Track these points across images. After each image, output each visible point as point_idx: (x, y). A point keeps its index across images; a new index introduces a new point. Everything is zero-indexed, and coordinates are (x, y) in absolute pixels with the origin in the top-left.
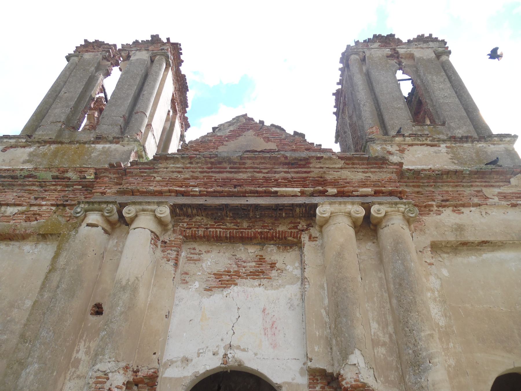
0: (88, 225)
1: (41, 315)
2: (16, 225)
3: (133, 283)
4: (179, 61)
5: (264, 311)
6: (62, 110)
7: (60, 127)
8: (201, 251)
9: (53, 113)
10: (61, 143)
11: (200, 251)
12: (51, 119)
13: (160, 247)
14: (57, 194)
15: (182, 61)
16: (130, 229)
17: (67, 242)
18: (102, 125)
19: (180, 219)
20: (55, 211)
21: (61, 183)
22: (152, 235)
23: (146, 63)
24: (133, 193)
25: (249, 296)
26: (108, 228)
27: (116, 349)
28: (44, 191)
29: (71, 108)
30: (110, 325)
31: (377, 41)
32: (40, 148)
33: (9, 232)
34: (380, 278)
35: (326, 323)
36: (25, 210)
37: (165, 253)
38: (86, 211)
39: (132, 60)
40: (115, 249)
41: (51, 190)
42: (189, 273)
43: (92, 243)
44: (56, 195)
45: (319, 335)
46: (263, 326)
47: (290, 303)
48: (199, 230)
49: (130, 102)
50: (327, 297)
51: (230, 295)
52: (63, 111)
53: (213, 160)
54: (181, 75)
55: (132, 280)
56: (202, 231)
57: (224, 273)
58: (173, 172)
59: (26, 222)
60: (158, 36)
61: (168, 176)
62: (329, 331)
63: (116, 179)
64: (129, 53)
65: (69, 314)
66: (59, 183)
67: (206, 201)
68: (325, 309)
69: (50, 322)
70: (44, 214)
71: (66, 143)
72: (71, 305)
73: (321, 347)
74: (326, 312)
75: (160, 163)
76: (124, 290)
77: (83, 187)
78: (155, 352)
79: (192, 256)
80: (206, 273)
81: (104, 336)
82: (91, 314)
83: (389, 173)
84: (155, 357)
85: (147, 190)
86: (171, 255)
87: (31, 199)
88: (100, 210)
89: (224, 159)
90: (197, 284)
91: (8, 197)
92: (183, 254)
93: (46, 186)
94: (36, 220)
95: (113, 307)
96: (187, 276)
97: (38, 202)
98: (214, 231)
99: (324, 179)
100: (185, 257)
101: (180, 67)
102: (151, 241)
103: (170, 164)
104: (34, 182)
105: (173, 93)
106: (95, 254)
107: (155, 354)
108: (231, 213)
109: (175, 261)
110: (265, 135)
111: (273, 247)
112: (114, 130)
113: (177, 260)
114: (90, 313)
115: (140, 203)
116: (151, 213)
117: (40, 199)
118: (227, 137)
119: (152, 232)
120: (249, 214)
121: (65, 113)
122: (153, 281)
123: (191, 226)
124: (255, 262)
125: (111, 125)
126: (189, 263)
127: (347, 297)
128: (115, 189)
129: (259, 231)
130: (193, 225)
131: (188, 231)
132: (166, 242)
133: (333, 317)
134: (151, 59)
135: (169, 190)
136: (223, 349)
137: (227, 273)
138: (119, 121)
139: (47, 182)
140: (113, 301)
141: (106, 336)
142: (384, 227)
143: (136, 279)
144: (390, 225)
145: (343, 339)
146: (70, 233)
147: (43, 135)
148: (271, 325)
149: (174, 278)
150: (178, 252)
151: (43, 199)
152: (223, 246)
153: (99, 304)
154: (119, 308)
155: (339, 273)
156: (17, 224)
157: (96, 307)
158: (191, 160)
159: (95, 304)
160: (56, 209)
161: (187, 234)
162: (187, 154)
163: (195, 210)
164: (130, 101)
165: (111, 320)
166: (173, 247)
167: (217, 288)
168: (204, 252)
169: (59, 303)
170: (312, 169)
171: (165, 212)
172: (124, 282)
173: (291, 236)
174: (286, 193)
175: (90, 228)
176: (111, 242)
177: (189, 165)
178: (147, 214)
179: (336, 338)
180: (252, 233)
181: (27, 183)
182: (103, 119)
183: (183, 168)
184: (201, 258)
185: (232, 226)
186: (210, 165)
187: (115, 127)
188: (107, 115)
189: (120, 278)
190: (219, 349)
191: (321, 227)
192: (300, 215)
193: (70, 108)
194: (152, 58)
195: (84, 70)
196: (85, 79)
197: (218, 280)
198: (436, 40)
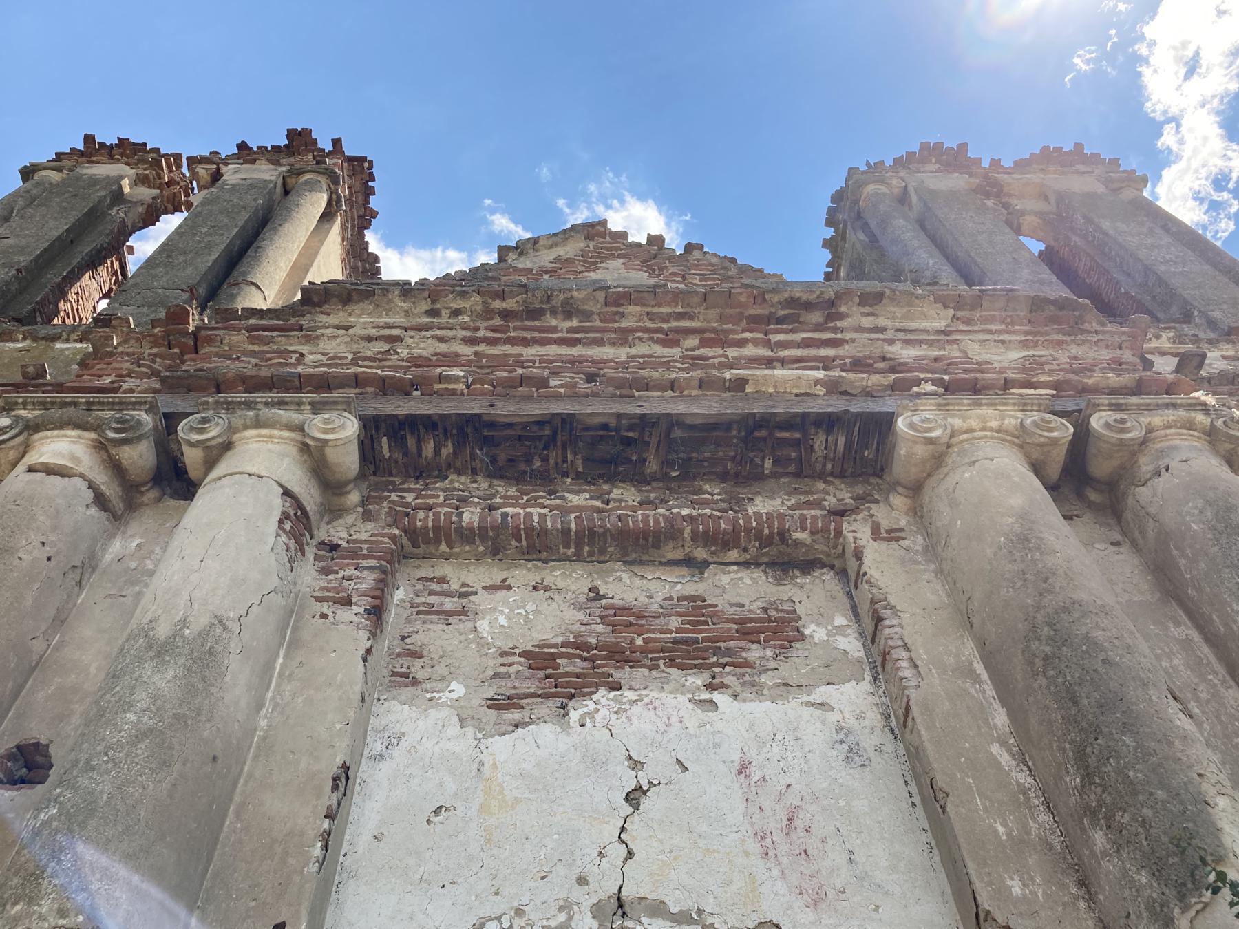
3: (204, 634)
5: (743, 769)
8: (468, 586)
11: (464, 585)
13: (312, 559)
19: (393, 483)
22: (288, 504)
25: (674, 720)
26: (111, 490)
29: (17, 270)
30: (83, 781)
31: (934, 161)
34: (1186, 643)
35: (1024, 791)
37: (331, 577)
42: (425, 653)
45: (1009, 835)
46: (752, 823)
47: (842, 742)
49: (215, 261)
50: (996, 705)
51: (598, 717)
53: (509, 304)
54: (366, 256)
55: (200, 621)
56: (472, 513)
57: (563, 650)
60: (307, 133)
62: (1044, 817)
67: (492, 405)
68: (1003, 743)
73: (1032, 879)
74: (1009, 751)
75: (323, 313)
80: (493, 650)
83: (1107, 347)
86: (356, 584)
89: (549, 299)
90: (458, 689)
92: (399, 594)
96: (419, 663)
99: (892, 363)
103: (360, 316)
106: (49, 559)
108: (579, 457)
109: (370, 599)
111: (737, 572)
116: (286, 434)
119: (287, 493)
120: (645, 461)
122: (280, 660)
123: (431, 501)
124: (679, 614)
126: (424, 622)
127: (1105, 661)
129: (685, 512)
130: (442, 498)
131: (421, 514)
133: (1064, 750)
134: (284, 184)
135: (356, 376)
136: (590, 915)
137: (572, 651)
141: (55, 824)
142: (1148, 476)
144: (1174, 465)
145: (1147, 812)
148: (785, 819)
149: (369, 651)
150: (385, 572)
152: (554, 569)
154: (131, 717)
155: (1041, 595)
157: (22, 762)
158: (433, 302)
159: (18, 747)
161: (419, 524)
163: (450, 445)
164: (214, 257)
165: (87, 762)
166: (365, 557)
167: (539, 700)
170: (848, 336)
173: (804, 529)
174: (775, 386)
176: (118, 544)
177: (426, 320)
178: (271, 437)
179: (1110, 818)
180: (661, 519)
184: (470, 605)
185: (586, 499)
186: (497, 321)
190: (570, 918)
191: (916, 489)
192: (824, 465)
194: (288, 180)
197: (541, 674)
198: (1094, 159)
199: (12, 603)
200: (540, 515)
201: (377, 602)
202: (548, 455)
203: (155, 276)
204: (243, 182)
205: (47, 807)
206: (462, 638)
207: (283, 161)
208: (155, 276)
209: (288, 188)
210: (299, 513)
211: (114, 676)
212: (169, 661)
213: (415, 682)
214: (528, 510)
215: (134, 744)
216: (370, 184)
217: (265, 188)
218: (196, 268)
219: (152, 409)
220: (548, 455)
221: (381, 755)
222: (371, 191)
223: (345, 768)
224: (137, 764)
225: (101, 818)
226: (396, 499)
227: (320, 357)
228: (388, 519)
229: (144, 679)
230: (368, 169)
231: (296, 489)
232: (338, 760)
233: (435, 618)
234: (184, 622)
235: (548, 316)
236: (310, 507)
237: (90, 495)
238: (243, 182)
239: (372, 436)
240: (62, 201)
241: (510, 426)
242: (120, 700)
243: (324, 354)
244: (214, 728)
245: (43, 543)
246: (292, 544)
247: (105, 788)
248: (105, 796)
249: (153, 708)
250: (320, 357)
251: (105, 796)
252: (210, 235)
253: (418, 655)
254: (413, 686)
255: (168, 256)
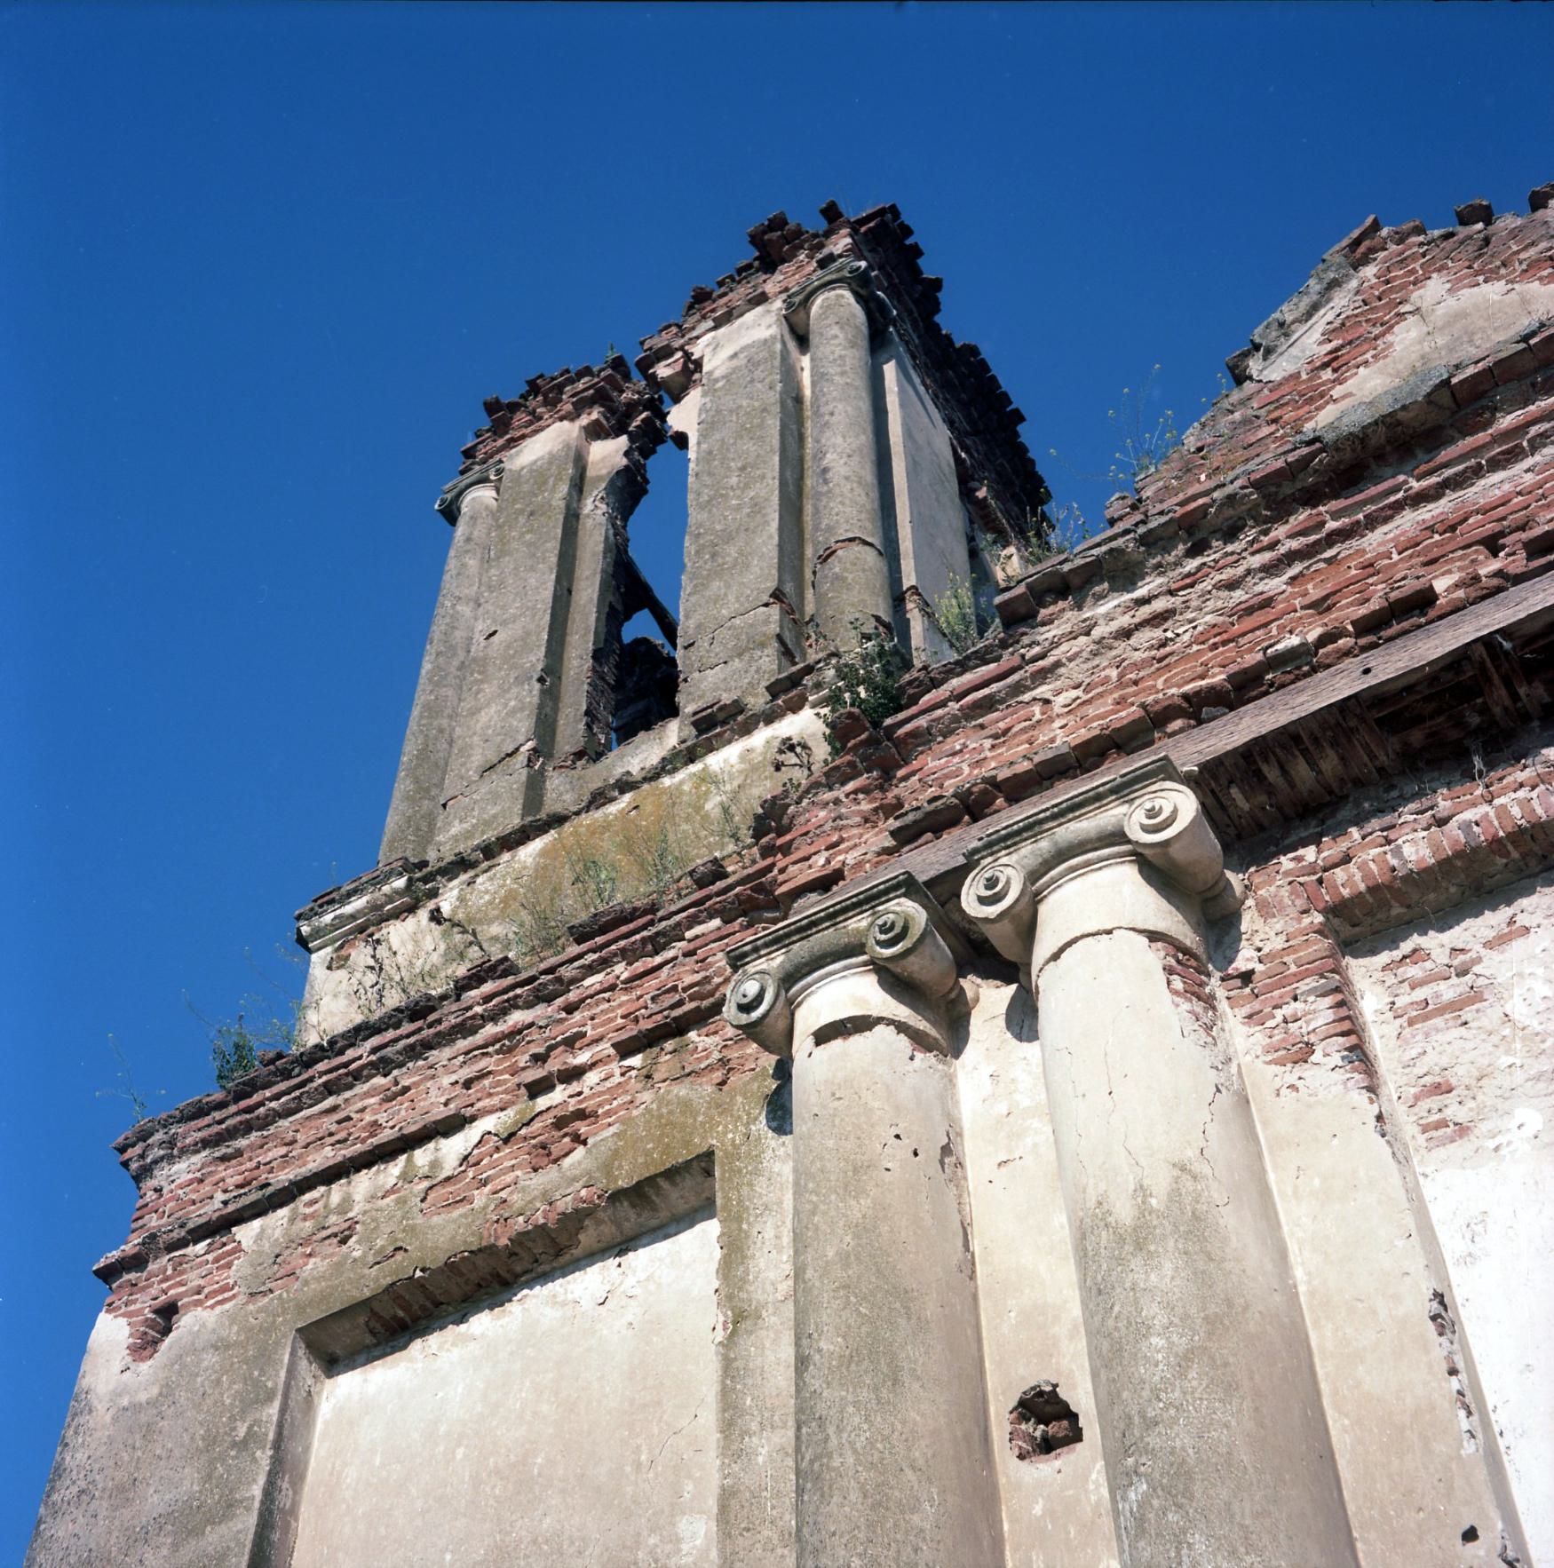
0: (824, 1035)
1: (779, 1551)
2: (505, 1201)
3: (1175, 1195)
4: (920, 288)
6: (506, 705)
7: (525, 771)
9: (475, 734)
10: (558, 820)
12: (477, 759)
13: (1228, 1010)
14: (624, 998)
15: (937, 284)
16: (1034, 977)
17: (757, 1172)
18: (696, 675)
20: (644, 1072)
21: (622, 943)
23: (778, 346)
24: (972, 806)
27: (1242, 1550)
28: (563, 1015)
30: (1153, 1440)
32: (476, 886)
33: (484, 1243)
36: (516, 1123)
38: (790, 978)
39: (710, 373)
40: (1002, 1108)
41: (592, 996)
42: (1453, 1082)
43: (876, 1104)
44: (620, 1006)
48: (1399, 847)
52: (513, 703)
55: (1160, 1184)
58: (1126, 634)
59: (535, 1170)
61: (1110, 666)
63: (861, 796)
64: (687, 355)
65: (913, 1468)
66: (613, 947)
67: (1367, 671)
69: (834, 1534)
70: (600, 1105)
71: (577, 813)
72: (904, 1423)
76: (1139, 1247)
77: (726, 922)
78: (1466, 1527)
79: (1421, 994)
81: (1144, 1504)
82: (1021, 1457)
84: (1482, 1553)
85: (1037, 759)
86: (1308, 1023)
87: (524, 1069)
88: (853, 949)
91: (422, 1104)
93: (566, 985)
94: (579, 1140)
95: (1120, 1350)
97: (554, 1065)
98: (1487, 814)
100: (1391, 1015)
101: (938, 319)
102: (1169, 983)
104: (505, 991)
105: (952, 445)
106: (916, 1154)
107: (1470, 1535)
109: (1341, 1040)
110: (1522, 256)
112: (757, 671)
113: (1351, 1030)
114: (1016, 1452)
115: (1031, 829)
117: (561, 1048)
118: (1325, 365)
119: (1154, 936)
121: (522, 709)
125: (740, 655)
128: (879, 838)
131: (1340, 874)
132: (1252, 972)
138: (767, 622)
139: (561, 965)
140: (1111, 1323)
141: (1155, 1502)
143: (1176, 1172)
146: (753, 1128)
147: (468, 835)
149: (1380, 1118)
151: (571, 1043)
153: (1041, 1394)
154: (1156, 1341)
156: (503, 1194)
158: (1190, 534)
160: (644, 1060)
162: (1161, 513)
165: (1143, 1416)
166: (1300, 977)
168: (1483, 952)
169: (840, 1430)
171: (1175, 812)
172: (1124, 1212)
175: (837, 1045)
181: (478, 1009)
182: (692, 649)
183: (1171, 593)
184: (1481, 981)
187: (759, 653)
188: (699, 626)
189: (1092, 1203)
193: (536, 676)
194: (794, 319)
195: (532, 514)
196: (549, 545)
199: (915, 1233)
200: (1519, 802)
201: (1353, 1040)
202: (1485, 703)
203: (716, 599)
204: (735, 363)
205: (1132, 1484)
206: (1495, 1039)
207: (770, 288)
208: (716, 599)
209: (801, 332)
210: (1180, 956)
211: (1100, 1292)
212: (1156, 1251)
213: (1462, 1130)
214: (1497, 802)
215: (1183, 1375)
216: (908, 242)
217: (772, 357)
218: (762, 556)
219: (909, 886)
220: (1485, 703)
221: (1470, 1255)
222: (916, 251)
223: (1439, 1297)
224: (1201, 1399)
225: (1203, 1480)
226: (1291, 865)
227: (1074, 694)
228: (1298, 902)
229: (1142, 1286)
230: (894, 221)
231: (1159, 925)
232: (1424, 1287)
233: (1438, 1021)
234: (1142, 1190)
235: (1374, 467)
236: (1200, 950)
237: (903, 1042)
238: (735, 363)
239: (1213, 791)
240: (522, 534)
241: (1410, 689)
242: (1130, 1323)
243: (1077, 687)
244: (1257, 1315)
245: (897, 1137)
246: (1198, 1007)
247: (1183, 1439)
248: (1191, 1451)
249: (1176, 1320)
250: (1074, 694)
251: (1191, 1451)
252: (747, 486)
253: (1444, 1088)
254: (1461, 1137)
255: (714, 555)
